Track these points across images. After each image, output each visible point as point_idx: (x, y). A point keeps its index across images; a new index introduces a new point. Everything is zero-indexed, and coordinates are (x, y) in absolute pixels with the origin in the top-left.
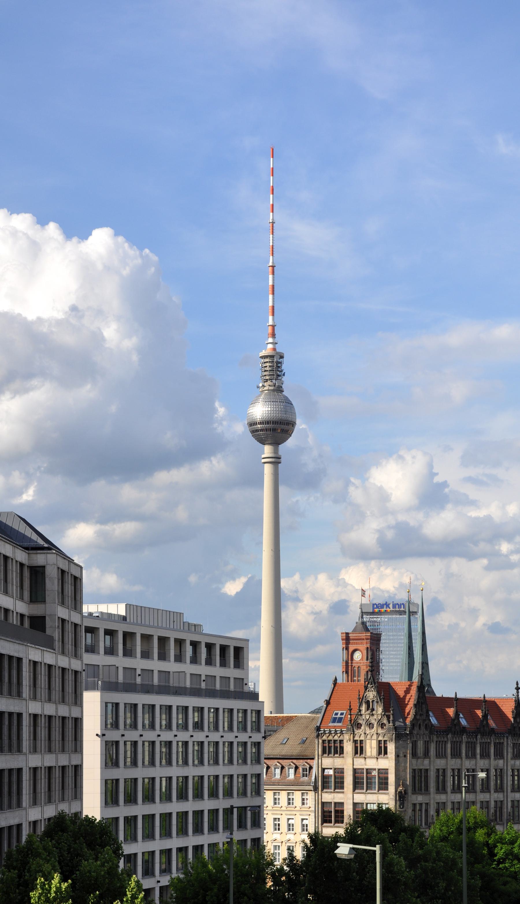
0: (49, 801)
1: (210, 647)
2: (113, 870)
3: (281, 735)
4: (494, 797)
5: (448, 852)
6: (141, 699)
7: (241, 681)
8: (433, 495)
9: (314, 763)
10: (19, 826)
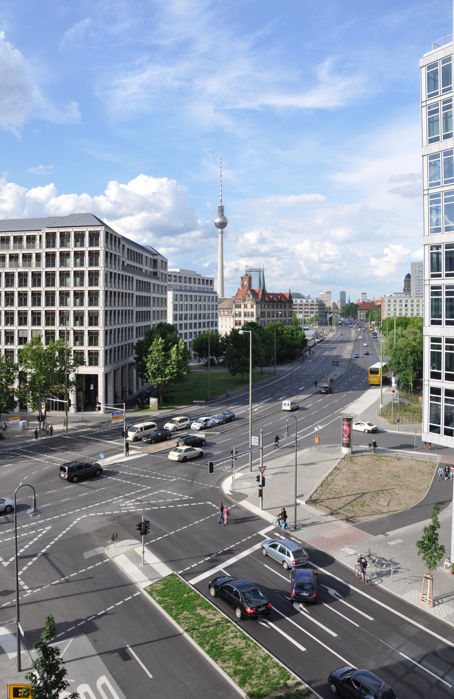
0: (158, 319)
1: (203, 280)
2: (176, 337)
3: (224, 303)
4: (283, 318)
5: (270, 332)
6: (184, 293)
7: (212, 289)
8: (262, 241)
9: (233, 310)
10: (150, 325)
